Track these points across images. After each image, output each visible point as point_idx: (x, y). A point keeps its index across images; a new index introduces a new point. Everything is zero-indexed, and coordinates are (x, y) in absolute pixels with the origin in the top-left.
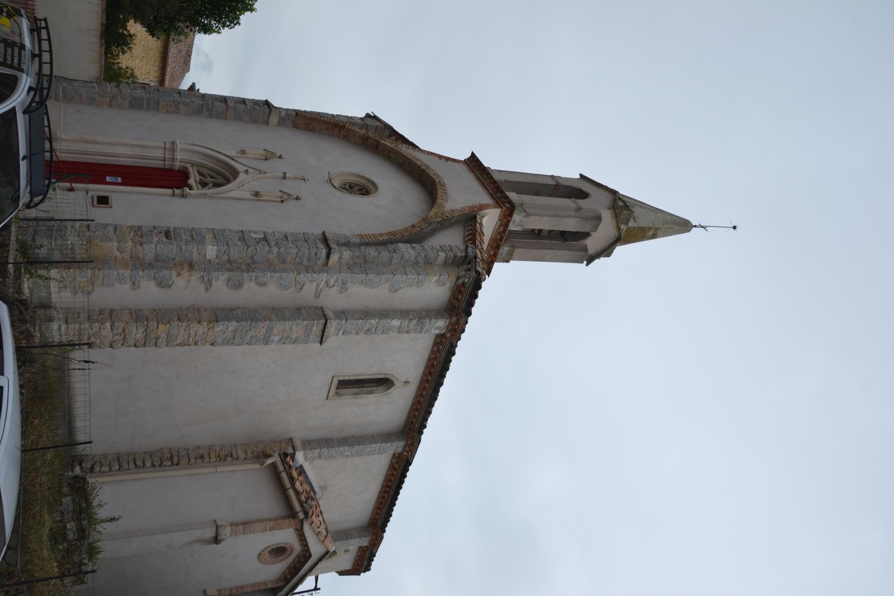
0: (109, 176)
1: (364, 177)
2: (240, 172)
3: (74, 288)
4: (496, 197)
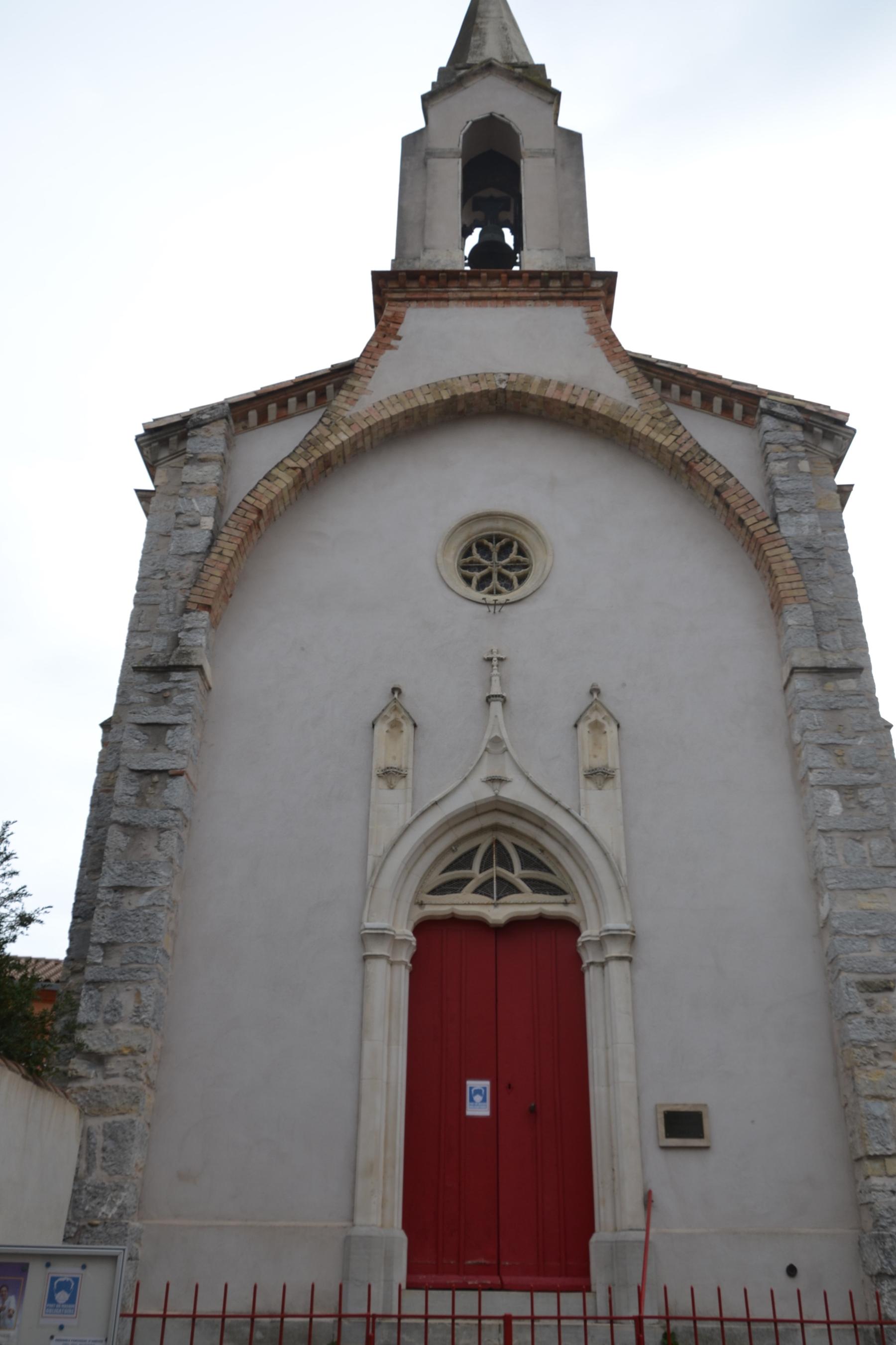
0: (462, 1107)
1: (455, 531)
2: (497, 795)
3: (112, 1224)
4: (560, 294)
